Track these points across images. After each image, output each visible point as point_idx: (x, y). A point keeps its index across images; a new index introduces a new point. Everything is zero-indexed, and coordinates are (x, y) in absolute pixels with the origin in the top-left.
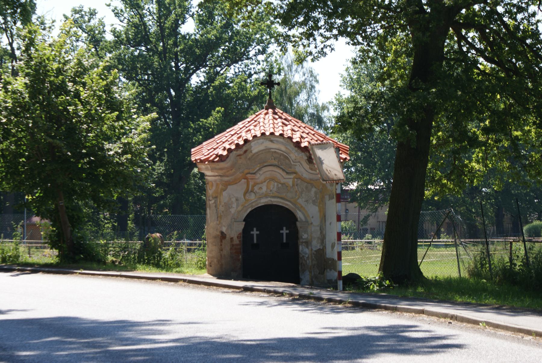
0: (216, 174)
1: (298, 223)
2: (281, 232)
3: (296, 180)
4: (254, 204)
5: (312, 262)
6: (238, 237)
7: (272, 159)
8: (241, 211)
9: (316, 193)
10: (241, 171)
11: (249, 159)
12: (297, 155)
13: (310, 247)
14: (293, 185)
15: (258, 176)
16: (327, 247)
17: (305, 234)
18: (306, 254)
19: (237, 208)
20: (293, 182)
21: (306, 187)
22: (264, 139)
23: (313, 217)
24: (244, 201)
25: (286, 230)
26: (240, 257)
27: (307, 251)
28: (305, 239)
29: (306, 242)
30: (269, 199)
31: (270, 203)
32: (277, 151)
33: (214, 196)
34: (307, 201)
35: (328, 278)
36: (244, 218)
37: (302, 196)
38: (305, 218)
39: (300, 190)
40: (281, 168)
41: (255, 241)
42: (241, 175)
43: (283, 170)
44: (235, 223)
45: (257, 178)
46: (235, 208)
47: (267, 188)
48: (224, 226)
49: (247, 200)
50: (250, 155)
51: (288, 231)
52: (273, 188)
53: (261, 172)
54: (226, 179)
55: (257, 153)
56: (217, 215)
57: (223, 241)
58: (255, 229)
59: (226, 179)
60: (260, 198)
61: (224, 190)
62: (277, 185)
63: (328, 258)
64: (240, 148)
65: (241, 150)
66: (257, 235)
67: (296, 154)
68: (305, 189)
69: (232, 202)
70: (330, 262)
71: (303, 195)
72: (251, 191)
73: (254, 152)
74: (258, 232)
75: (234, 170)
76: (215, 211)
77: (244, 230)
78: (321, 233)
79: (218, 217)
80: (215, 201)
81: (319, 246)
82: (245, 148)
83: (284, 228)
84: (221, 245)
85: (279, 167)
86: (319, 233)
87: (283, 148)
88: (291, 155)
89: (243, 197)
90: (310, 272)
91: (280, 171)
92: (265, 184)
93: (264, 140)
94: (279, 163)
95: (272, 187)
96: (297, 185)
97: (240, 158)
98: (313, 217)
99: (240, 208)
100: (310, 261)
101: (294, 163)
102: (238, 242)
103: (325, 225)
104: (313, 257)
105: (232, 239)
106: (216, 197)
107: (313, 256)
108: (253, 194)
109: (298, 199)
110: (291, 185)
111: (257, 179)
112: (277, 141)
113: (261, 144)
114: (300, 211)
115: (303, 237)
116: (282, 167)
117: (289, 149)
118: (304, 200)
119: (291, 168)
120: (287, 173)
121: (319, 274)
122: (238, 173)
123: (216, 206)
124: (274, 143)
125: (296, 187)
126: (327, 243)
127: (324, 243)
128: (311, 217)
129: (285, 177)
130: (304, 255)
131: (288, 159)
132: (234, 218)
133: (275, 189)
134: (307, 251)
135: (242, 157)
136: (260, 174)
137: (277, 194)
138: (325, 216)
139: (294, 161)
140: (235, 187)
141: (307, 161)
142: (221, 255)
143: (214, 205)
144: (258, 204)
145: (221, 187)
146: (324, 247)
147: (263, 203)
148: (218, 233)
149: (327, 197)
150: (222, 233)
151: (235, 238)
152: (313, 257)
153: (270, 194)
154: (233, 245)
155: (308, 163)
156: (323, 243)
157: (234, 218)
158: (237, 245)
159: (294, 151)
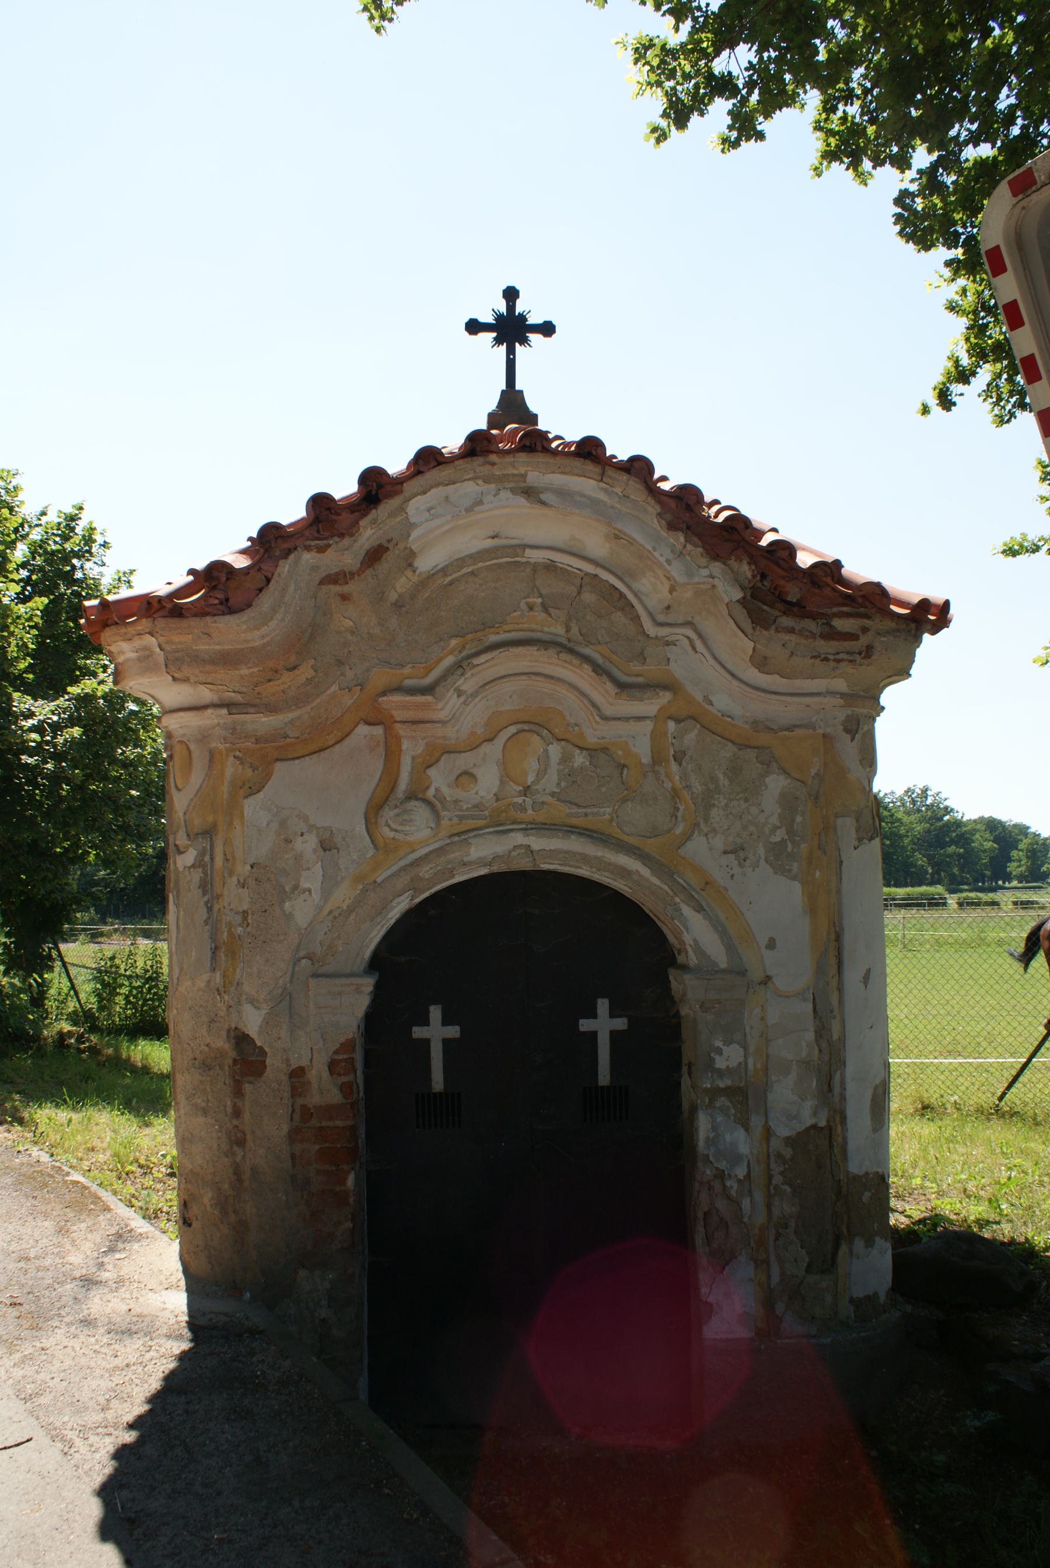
0: (206, 694)
1: (678, 982)
2: (585, 1025)
3: (671, 725)
4: (425, 871)
5: (769, 1206)
6: (332, 1066)
7: (531, 608)
8: (350, 910)
9: (788, 803)
10: (350, 674)
11: (398, 605)
12: (680, 578)
13: (756, 1121)
14: (658, 759)
15: (448, 704)
16: (850, 1113)
17: (728, 1043)
18: (736, 1159)
19: (327, 893)
20: (657, 737)
21: (734, 771)
22: (487, 481)
23: (771, 945)
24: (371, 852)
25: (594, 1015)
26: (350, 1181)
27: (741, 1142)
28: (729, 1071)
29: (728, 1092)
30: (519, 839)
31: (524, 864)
32: (558, 557)
33: (197, 823)
34: (736, 850)
35: (859, 1293)
36: (368, 953)
37: (706, 820)
38: (730, 948)
39: (698, 787)
40: (587, 659)
41: (438, 1081)
42: (348, 701)
43: (598, 669)
44: (312, 982)
45: (442, 715)
46: (316, 896)
47: (506, 776)
48: (252, 1002)
49: (384, 848)
50: (403, 584)
51: (621, 1024)
52: (541, 774)
53: (468, 683)
54: (264, 722)
55: (444, 571)
56: (214, 937)
57: (247, 1088)
58: (435, 1013)
59: (264, 722)
60: (462, 836)
61: (252, 792)
62: (566, 759)
63: (857, 1178)
64: (342, 535)
65: (346, 541)
66: (446, 1042)
67: (676, 571)
68: (724, 781)
69: (298, 857)
70: (866, 1196)
71: (714, 813)
72: (412, 796)
73: (425, 563)
74: (453, 1032)
75: (305, 672)
76: (203, 913)
77: (372, 1020)
78: (822, 1032)
79: (215, 951)
80: (202, 854)
81: (808, 1115)
82: (368, 535)
83: (603, 1006)
84: (237, 1113)
85: (572, 651)
86: (810, 1035)
87: (596, 544)
88: (645, 584)
89: (361, 828)
90: (761, 1264)
91: (582, 677)
92: (494, 750)
93: (484, 487)
94: (575, 630)
95: (532, 766)
96: (679, 757)
97: (345, 597)
98: (771, 945)
99: (343, 895)
100: (759, 1196)
101: (663, 632)
102: (335, 1097)
103: (840, 989)
104: (777, 1179)
105: (298, 1074)
106: (209, 833)
107: (776, 1168)
108: (420, 814)
109: (687, 837)
110: (646, 759)
111: (443, 723)
112: (563, 494)
113: (469, 510)
114: (699, 909)
115: (720, 1063)
116: (587, 651)
117: (632, 542)
118: (718, 842)
119: (642, 657)
120: (622, 687)
121: (809, 1269)
122: (334, 688)
123: (205, 885)
124: (543, 503)
125: (674, 766)
126: (851, 1087)
127: (837, 1090)
128: (763, 941)
129: (609, 711)
130: (722, 1165)
131: (627, 607)
132: (310, 957)
133: (551, 781)
134: (741, 1142)
135: (351, 588)
136: (460, 693)
137: (561, 811)
138: (838, 938)
139: (661, 618)
140: (312, 768)
141: (741, 614)
142: (237, 1172)
143: (197, 875)
144: (452, 874)
145: (231, 769)
146: (839, 1115)
147: (482, 862)
148: (221, 1043)
149: (847, 827)
150: (241, 1039)
151: (318, 1073)
152: (777, 1179)
153: (523, 808)
154: (306, 1113)
155: (747, 624)
156: (830, 1089)
157: (310, 957)
158: (328, 1111)
159: (662, 555)
